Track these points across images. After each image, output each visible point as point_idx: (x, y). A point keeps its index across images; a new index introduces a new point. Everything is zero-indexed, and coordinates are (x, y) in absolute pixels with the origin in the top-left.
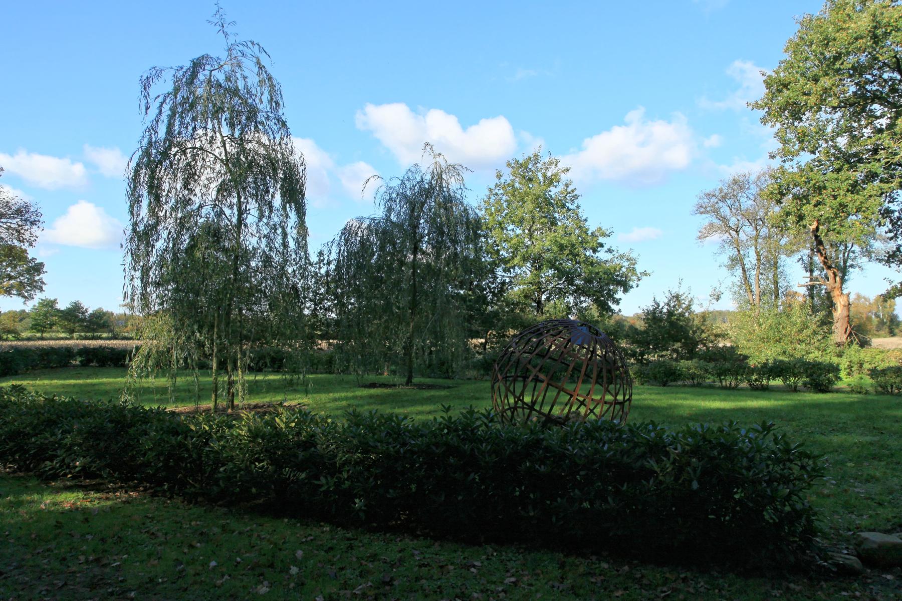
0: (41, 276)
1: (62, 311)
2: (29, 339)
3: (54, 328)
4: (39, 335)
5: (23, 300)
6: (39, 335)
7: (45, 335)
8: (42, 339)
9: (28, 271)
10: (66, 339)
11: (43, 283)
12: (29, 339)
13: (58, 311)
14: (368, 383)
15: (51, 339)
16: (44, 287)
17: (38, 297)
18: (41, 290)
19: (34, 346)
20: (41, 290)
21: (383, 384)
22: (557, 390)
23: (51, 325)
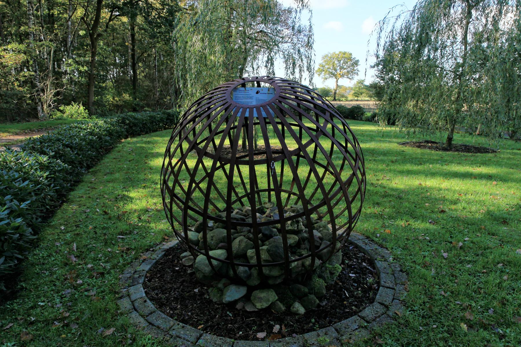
0: (358, 67)
1: (367, 86)
2: (351, 101)
3: (363, 94)
4: (356, 98)
5: (349, 80)
6: (356, 98)
7: (359, 99)
8: (357, 100)
9: (352, 65)
10: (368, 101)
11: (358, 71)
12: (351, 101)
13: (366, 86)
14: (150, 321)
15: (362, 101)
16: (359, 73)
17: (356, 78)
18: (357, 74)
19: (490, 168)
20: (357, 74)
21: (475, 178)
22: (324, 170)
23: (361, 94)
